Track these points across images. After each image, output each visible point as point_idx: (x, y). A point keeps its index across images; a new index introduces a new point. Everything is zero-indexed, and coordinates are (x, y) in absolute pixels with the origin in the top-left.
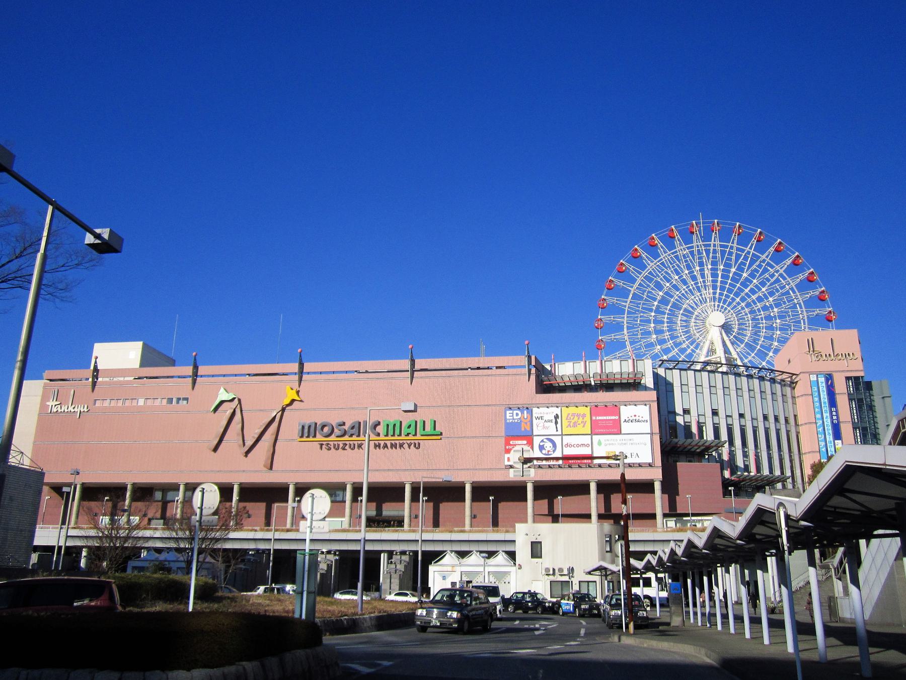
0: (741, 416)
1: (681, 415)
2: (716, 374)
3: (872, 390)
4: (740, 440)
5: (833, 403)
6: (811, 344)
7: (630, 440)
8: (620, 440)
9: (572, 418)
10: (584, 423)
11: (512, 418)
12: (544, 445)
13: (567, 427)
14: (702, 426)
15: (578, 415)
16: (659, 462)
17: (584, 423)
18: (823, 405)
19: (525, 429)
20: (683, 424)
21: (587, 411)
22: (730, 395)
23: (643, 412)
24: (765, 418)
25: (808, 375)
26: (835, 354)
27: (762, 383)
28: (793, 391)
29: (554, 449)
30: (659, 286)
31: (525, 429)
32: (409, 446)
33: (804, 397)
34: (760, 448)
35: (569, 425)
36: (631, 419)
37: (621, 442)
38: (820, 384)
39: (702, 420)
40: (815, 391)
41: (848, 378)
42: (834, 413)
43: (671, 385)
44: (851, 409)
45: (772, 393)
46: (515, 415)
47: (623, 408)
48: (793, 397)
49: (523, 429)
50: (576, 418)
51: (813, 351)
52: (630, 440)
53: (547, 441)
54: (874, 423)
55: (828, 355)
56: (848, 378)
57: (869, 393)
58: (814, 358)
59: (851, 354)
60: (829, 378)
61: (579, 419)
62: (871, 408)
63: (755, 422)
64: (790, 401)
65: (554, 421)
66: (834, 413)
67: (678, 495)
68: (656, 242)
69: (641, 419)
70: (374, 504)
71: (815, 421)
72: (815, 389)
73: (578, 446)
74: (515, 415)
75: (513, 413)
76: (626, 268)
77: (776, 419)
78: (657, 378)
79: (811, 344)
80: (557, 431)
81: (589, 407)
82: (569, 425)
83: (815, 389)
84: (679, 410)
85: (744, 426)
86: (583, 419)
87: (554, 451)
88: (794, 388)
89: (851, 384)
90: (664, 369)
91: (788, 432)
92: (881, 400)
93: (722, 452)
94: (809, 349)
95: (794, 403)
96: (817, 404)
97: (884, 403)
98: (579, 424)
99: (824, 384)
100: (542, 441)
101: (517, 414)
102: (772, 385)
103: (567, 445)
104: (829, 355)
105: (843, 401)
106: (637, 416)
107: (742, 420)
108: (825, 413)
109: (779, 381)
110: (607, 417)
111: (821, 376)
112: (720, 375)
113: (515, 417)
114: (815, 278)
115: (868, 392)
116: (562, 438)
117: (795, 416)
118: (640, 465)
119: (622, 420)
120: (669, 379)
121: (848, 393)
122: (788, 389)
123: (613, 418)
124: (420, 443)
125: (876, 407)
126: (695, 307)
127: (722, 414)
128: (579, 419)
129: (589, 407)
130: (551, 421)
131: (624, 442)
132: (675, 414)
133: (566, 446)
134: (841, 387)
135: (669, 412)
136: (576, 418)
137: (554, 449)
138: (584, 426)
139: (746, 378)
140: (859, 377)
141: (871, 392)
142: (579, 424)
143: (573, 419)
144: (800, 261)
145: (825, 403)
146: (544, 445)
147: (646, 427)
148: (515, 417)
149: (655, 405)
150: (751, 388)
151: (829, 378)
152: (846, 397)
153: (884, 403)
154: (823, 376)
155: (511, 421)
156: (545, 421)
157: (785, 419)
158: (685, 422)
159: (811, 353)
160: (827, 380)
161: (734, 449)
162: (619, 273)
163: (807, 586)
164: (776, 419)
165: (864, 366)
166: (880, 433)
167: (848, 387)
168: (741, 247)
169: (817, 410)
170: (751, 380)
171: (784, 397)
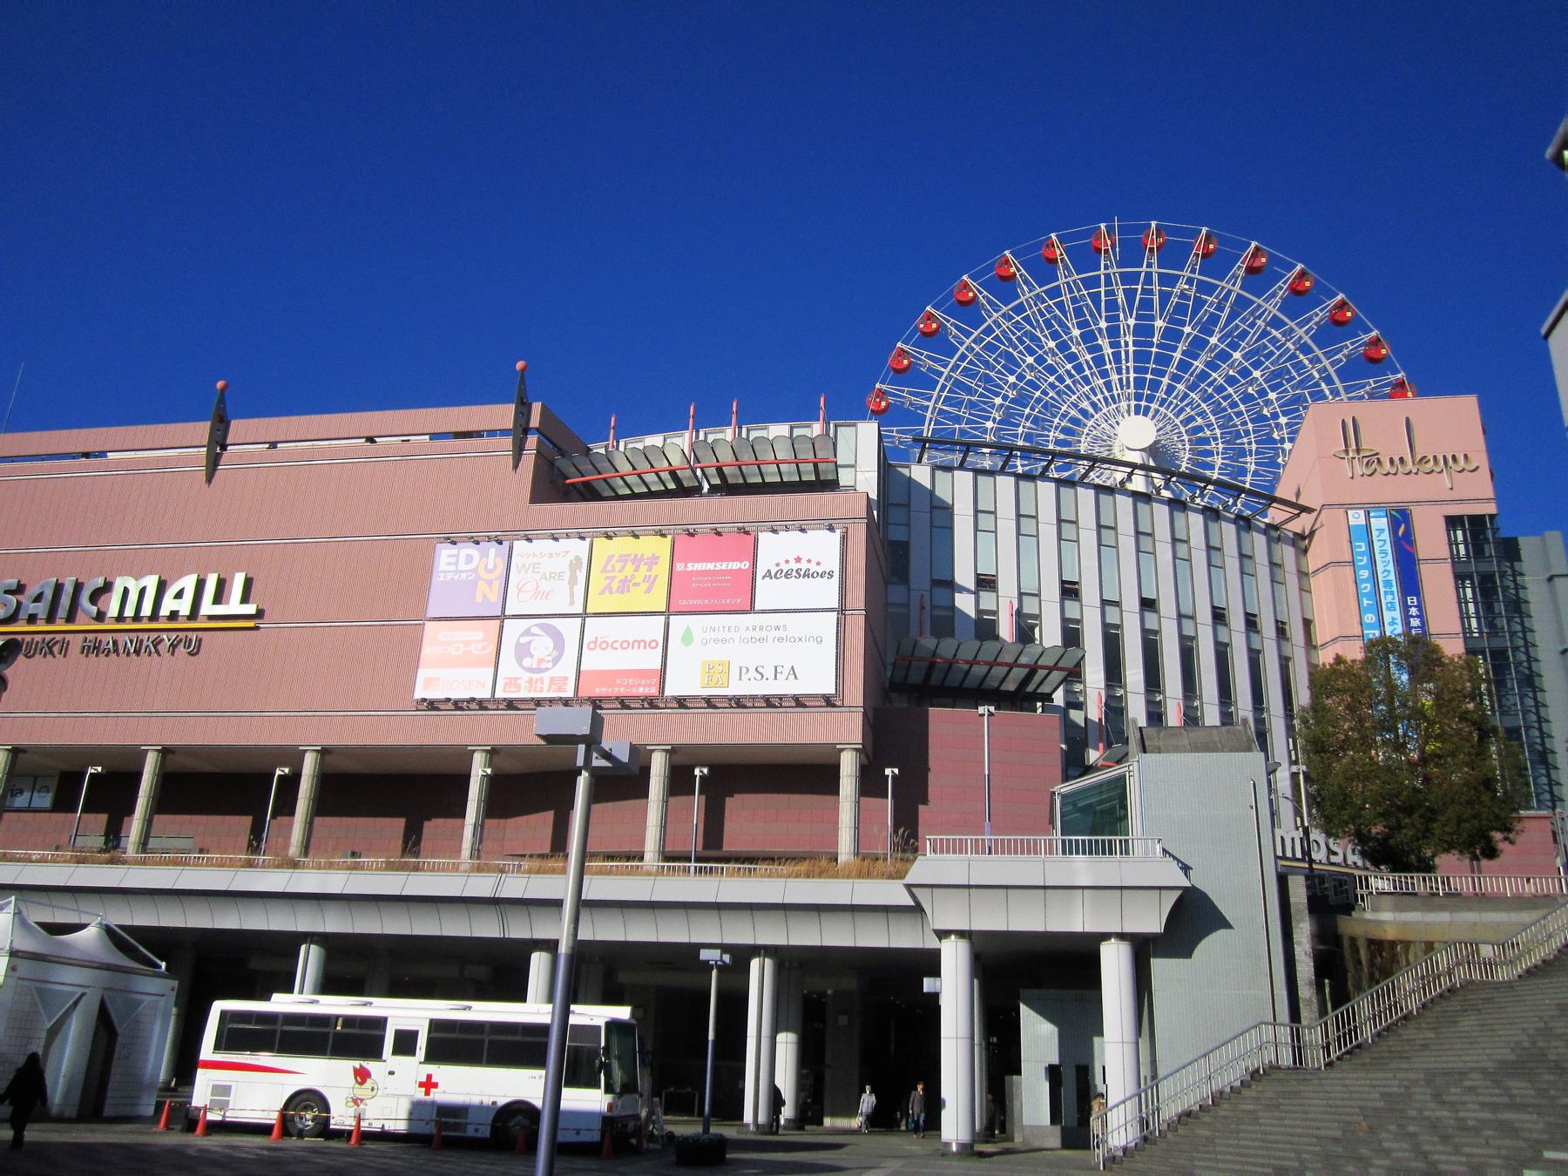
0: (1148, 605)
1: (969, 591)
2: (1079, 488)
3: (1519, 560)
4: (1142, 670)
5: (1409, 581)
6: (1352, 432)
7: (777, 628)
8: (747, 628)
9: (618, 566)
10: (651, 581)
11: (453, 567)
12: (530, 643)
13: (602, 593)
14: (1032, 627)
15: (637, 561)
16: (855, 693)
17: (651, 581)
18: (1382, 590)
19: (484, 596)
20: (972, 614)
21: (661, 547)
22: (1116, 547)
23: (822, 547)
24: (1219, 616)
25: (1342, 511)
26: (1418, 457)
27: (1213, 526)
28: (1303, 560)
29: (555, 654)
30: (1011, 363)
31: (484, 596)
32: (173, 646)
33: (1330, 570)
34: (1201, 697)
35: (608, 588)
36: (785, 568)
37: (749, 634)
38: (1375, 534)
39: (1030, 607)
40: (1362, 554)
41: (1452, 522)
42: (1414, 611)
43: (947, 510)
44: (1461, 601)
45: (1242, 556)
46: (462, 558)
47: (765, 538)
48: (1303, 574)
49: (479, 599)
50: (630, 568)
51: (1358, 451)
52: (777, 628)
53: (541, 633)
54: (1550, 784)
55: (1397, 461)
56: (1452, 522)
57: (1512, 567)
58: (1359, 469)
59: (1462, 458)
60: (1400, 520)
61: (636, 570)
62: (1517, 607)
63: (1187, 623)
64: (1292, 580)
65: (567, 575)
66: (1414, 611)
67: (925, 801)
68: (1013, 269)
69: (813, 568)
70: (103, 818)
71: (1360, 634)
72: (1360, 547)
73: (625, 645)
74: (462, 558)
75: (457, 556)
76: (941, 325)
77: (1251, 622)
78: (909, 491)
79: (1352, 432)
80: (572, 603)
81: (669, 537)
82: (608, 588)
83: (1360, 547)
84: (964, 575)
85: (1156, 632)
86: (650, 570)
87: (556, 661)
88: (1305, 551)
89: (1469, 592)
90: (928, 469)
91: (1284, 663)
92: (1545, 585)
93: (1085, 699)
94: (1346, 446)
95: (1304, 589)
96: (1367, 587)
97: (1553, 594)
98: (637, 584)
99: (1386, 536)
100: (527, 632)
101: (469, 559)
102: (1243, 534)
103: (595, 643)
104: (1402, 460)
105: (1438, 581)
106: (804, 561)
107: (1149, 616)
108: (1389, 609)
109: (1263, 526)
110: (725, 564)
111: (1378, 514)
112: (1092, 492)
113: (462, 566)
114: (1384, 351)
115: (1508, 564)
116: (583, 626)
117: (1307, 623)
118: (799, 701)
119: (760, 572)
120: (942, 492)
121: (1464, 633)
122: (1287, 553)
123: (735, 565)
124: (201, 640)
125: (1531, 605)
126: (1091, 410)
127: (1090, 594)
128: (636, 570)
129: (669, 537)
130: (560, 575)
131: (758, 634)
132: (950, 585)
133: (592, 646)
134: (1432, 541)
135: (937, 583)
136: (630, 568)
137: (555, 654)
138: (648, 591)
139: (1167, 508)
140: (1484, 516)
141: (1516, 564)
142: (637, 584)
143: (622, 569)
144: (1349, 314)
145: (1388, 583)
146: (530, 643)
147: (828, 593)
148: (462, 566)
149: (859, 534)
150: (1181, 535)
151: (1400, 520)
152: (1446, 571)
153: (1553, 594)
154: (1383, 514)
155: (450, 576)
156: (544, 577)
157: (1277, 628)
158: (979, 611)
159: (1351, 455)
160: (1394, 524)
161: (1122, 692)
162: (925, 339)
163: (1245, 1092)
164: (1251, 622)
165: (1496, 488)
166: (1543, 674)
167: (1452, 543)
168: (1209, 280)
169: (1365, 602)
170: (1183, 515)
171: (1277, 570)
